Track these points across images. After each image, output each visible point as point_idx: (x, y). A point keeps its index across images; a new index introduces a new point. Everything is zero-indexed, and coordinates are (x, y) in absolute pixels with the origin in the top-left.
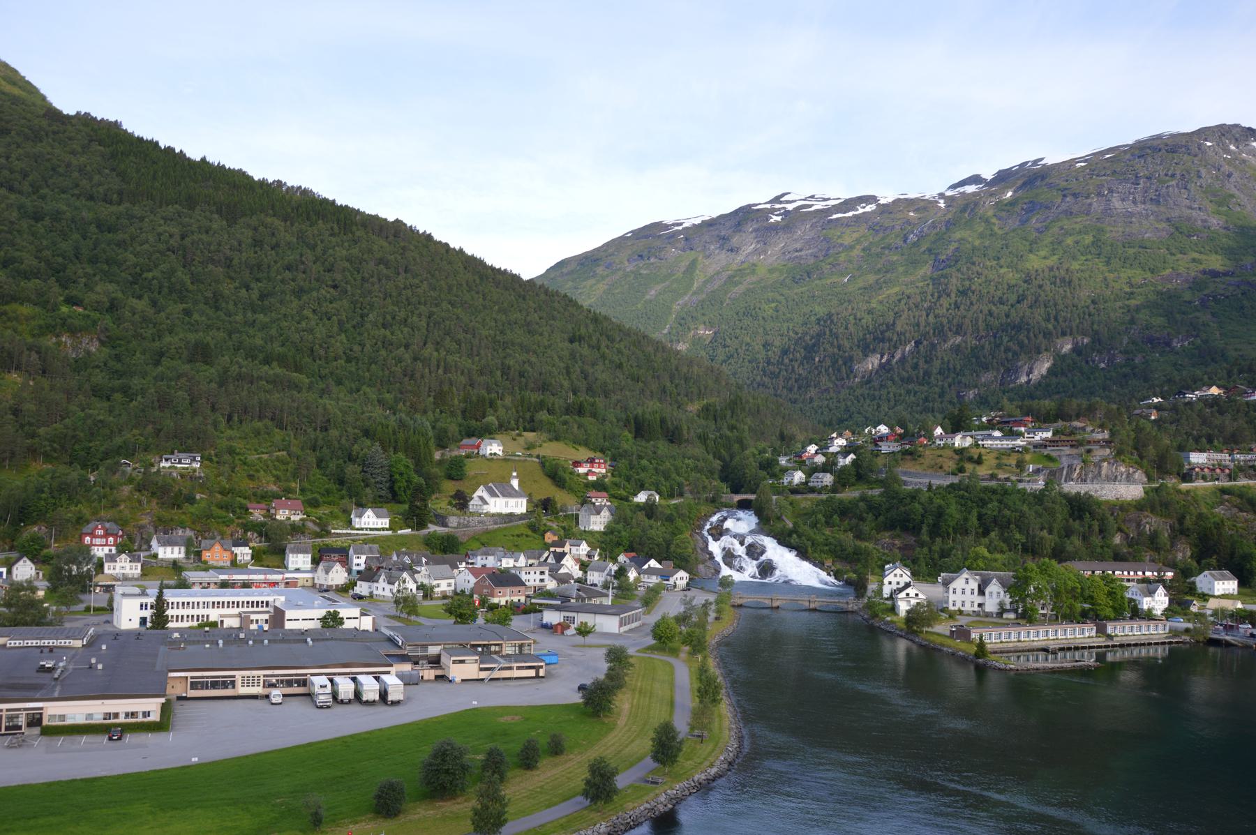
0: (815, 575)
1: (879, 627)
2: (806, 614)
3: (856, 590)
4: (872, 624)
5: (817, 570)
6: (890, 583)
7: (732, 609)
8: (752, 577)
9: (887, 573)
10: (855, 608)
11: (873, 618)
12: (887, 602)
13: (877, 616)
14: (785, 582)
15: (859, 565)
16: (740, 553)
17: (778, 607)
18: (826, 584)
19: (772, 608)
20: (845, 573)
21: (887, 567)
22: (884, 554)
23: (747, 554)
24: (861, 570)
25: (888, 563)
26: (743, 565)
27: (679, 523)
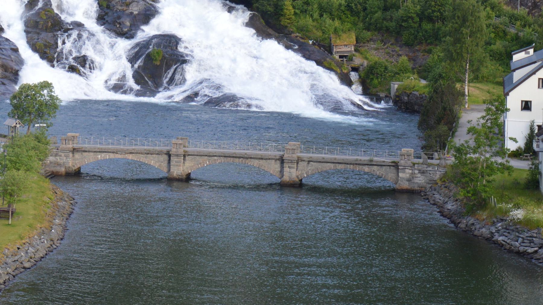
0: (305, 82)
1: (489, 240)
2: (272, 197)
3: (423, 125)
4: (468, 231)
5: (311, 66)
6: (527, 106)
7: (48, 184)
8: (117, 88)
9: (517, 75)
10: (420, 180)
11: (471, 211)
12: (515, 163)
13: (483, 204)
14: (213, 102)
15: (438, 52)
16: (79, 18)
17: (188, 178)
18: (337, 108)
19: (170, 180)
20: (396, 75)
21: (518, 57)
22: (513, 18)
23: (101, 19)
24: (441, 68)
25: (524, 45)
26: (89, 51)
27: (492, 130)
